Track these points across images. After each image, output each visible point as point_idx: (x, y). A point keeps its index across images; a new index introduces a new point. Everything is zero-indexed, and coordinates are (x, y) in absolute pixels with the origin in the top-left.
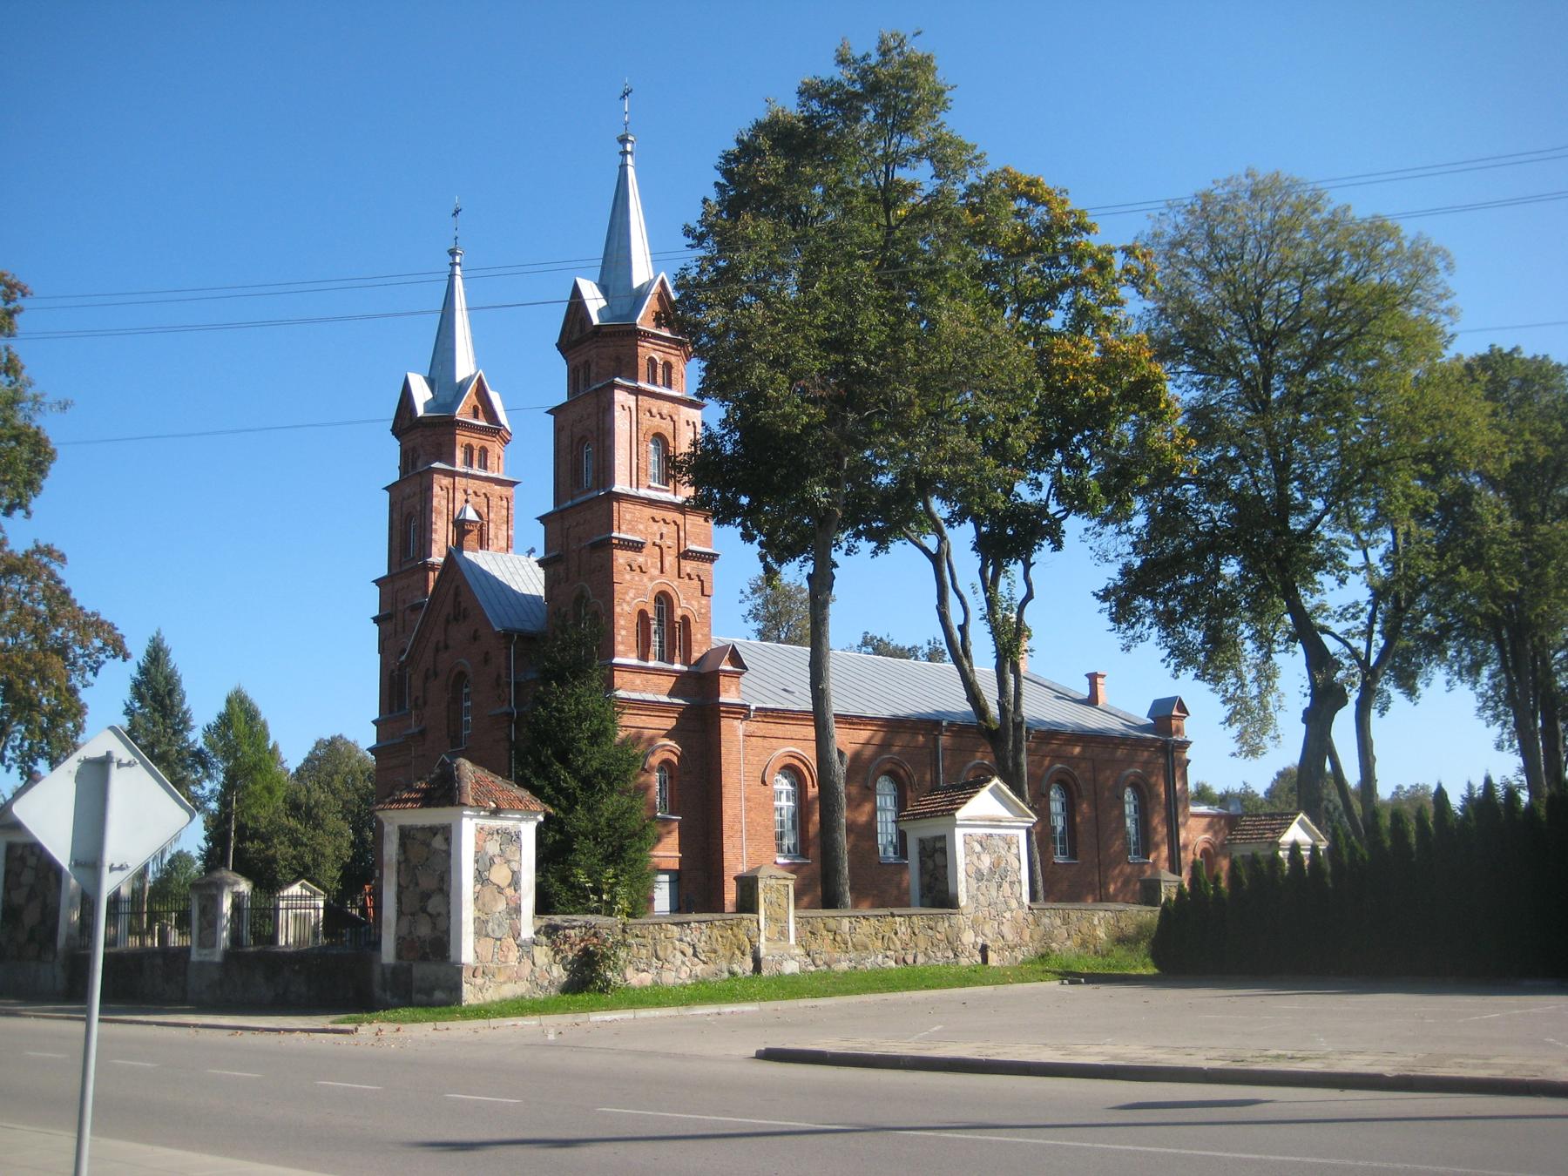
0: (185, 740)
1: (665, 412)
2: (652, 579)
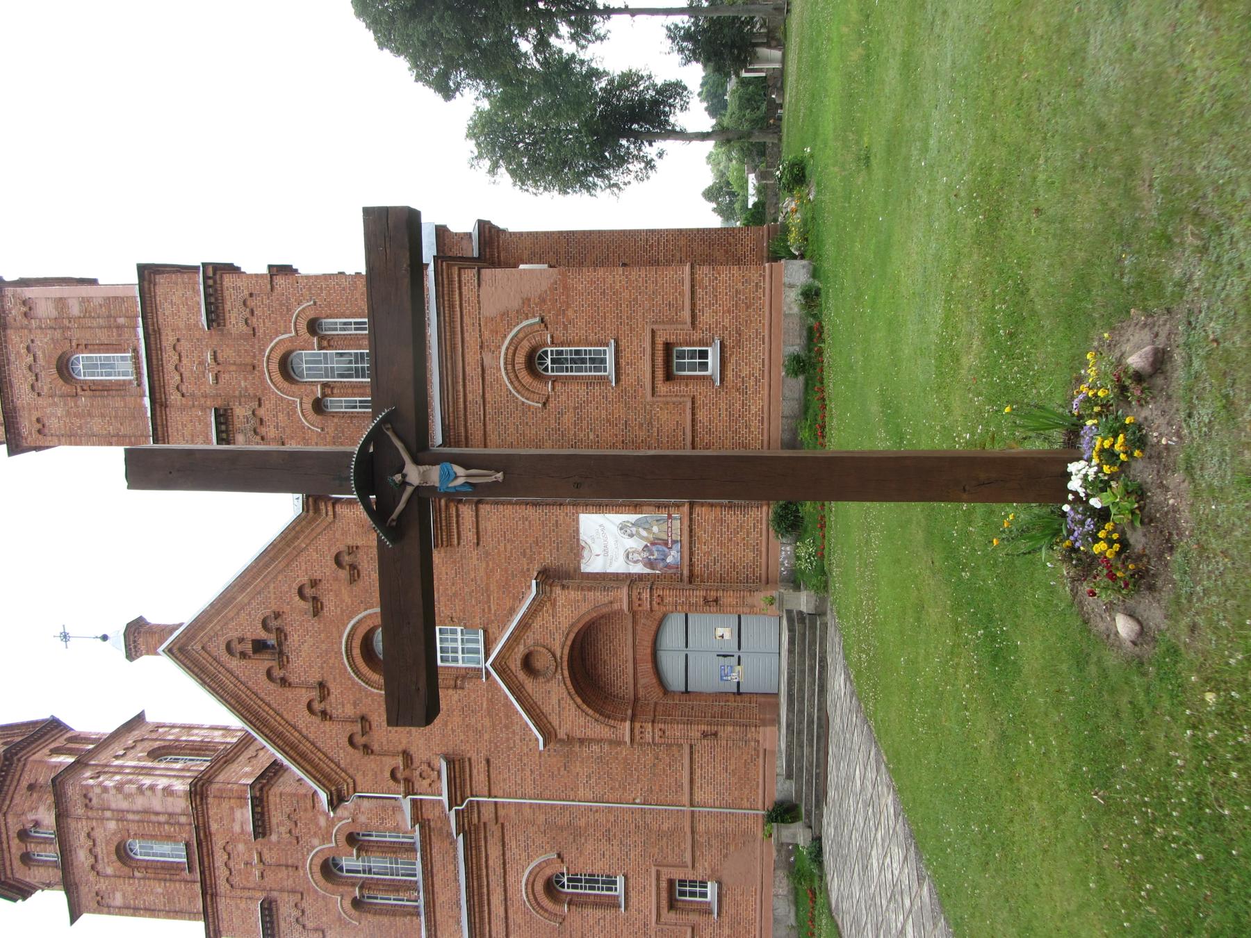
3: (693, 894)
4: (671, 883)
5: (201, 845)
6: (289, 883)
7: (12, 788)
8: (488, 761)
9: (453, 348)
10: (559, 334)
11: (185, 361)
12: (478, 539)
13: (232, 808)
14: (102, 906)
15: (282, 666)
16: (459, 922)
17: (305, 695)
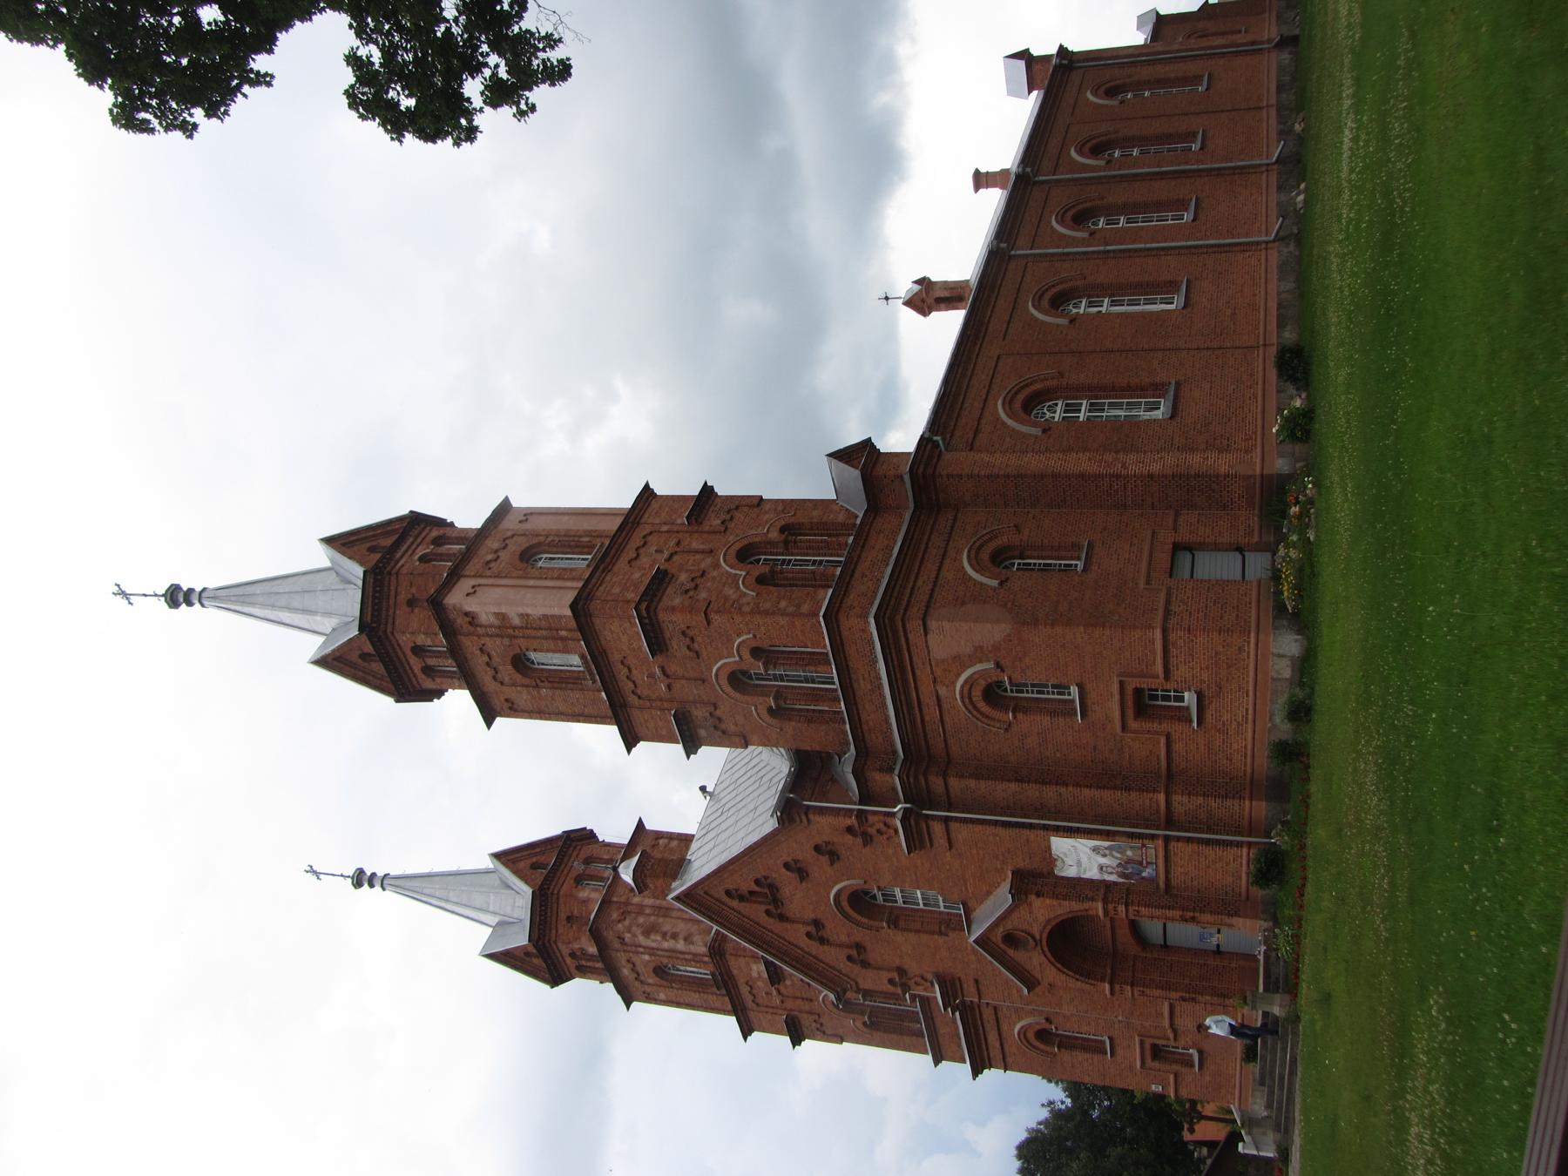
1: (496, 545)
2: (716, 565)
3: (1167, 698)
4: (1138, 692)
5: (598, 657)
6: (807, 1007)
8: (976, 981)
9: (905, 681)
10: (1017, 678)
11: (634, 672)
13: (748, 964)
14: (514, 711)
15: (777, 908)
16: (959, 1045)
17: (803, 929)
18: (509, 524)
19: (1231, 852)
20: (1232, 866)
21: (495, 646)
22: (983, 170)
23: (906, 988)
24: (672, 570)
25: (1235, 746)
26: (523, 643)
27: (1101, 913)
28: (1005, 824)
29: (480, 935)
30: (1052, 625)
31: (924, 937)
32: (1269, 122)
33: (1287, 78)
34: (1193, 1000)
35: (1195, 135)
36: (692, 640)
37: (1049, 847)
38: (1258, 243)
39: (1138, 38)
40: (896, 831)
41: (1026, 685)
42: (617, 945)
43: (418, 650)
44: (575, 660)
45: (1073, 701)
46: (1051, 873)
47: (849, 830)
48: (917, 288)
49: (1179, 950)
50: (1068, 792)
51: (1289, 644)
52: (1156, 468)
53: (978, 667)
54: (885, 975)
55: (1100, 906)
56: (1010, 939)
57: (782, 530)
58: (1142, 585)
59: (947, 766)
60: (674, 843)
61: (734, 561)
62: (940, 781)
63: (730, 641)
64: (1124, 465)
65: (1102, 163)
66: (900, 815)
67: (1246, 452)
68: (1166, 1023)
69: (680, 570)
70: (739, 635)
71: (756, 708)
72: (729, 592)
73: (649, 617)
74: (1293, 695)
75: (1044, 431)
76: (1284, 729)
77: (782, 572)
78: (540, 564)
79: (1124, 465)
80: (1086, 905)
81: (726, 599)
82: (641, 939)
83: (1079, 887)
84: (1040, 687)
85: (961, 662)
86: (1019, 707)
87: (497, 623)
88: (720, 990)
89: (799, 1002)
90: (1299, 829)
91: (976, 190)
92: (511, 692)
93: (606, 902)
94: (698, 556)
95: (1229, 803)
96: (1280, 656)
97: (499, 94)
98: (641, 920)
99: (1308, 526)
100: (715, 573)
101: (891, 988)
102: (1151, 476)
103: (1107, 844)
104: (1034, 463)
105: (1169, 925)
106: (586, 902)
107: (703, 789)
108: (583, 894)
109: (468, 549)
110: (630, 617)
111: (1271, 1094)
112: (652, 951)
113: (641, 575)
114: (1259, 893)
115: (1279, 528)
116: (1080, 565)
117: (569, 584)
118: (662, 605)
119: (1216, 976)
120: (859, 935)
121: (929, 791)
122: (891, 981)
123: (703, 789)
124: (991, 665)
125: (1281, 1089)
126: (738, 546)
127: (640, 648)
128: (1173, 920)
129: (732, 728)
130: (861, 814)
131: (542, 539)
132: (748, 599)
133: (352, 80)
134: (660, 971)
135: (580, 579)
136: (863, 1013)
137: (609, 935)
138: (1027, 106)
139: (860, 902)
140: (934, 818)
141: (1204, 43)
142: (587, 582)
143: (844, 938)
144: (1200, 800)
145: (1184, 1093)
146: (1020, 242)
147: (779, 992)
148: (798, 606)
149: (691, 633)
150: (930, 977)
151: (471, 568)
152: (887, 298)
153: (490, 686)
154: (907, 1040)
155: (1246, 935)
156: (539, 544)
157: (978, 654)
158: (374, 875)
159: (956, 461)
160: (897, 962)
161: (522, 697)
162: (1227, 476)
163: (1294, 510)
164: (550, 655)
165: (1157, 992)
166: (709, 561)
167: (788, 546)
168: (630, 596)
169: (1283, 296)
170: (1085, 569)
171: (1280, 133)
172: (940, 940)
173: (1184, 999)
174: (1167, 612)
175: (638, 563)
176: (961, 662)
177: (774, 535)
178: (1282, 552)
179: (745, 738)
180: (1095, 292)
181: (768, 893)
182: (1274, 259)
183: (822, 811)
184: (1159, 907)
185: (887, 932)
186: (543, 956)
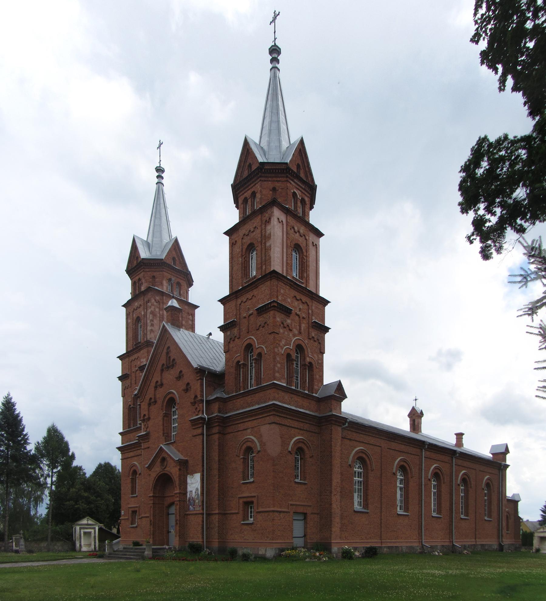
0: (25, 448)
1: (301, 231)
2: (294, 336)
4: (252, 502)
5: (255, 284)
7: (153, 270)
8: (149, 448)
12: (195, 436)
16: (127, 442)
17: (159, 380)
18: (312, 237)
19: (201, 536)
20: (196, 536)
21: (257, 233)
22: (463, 436)
23: (143, 421)
24: (291, 316)
25: (236, 536)
26: (259, 249)
27: (176, 492)
28: (203, 456)
29: (143, 234)
30: (273, 471)
31: (162, 427)
32: (469, 542)
33: (487, 548)
34: (151, 524)
35: (467, 516)
36: (263, 327)
37: (197, 473)
38: (422, 539)
39: (510, 493)
40: (197, 415)
41: (253, 462)
42: (146, 300)
43: (254, 194)
44: (254, 273)
45: (249, 479)
46: (188, 474)
47: (196, 397)
48: (419, 412)
49: (168, 519)
50: (216, 479)
51: (270, 553)
52: (334, 506)
53: (258, 444)
54: (146, 413)
55: (178, 491)
56: (164, 460)
57: (310, 363)
58: (290, 503)
59: (222, 434)
60: (190, 322)
61: (297, 343)
62: (217, 431)
63: (263, 343)
64: (336, 495)
65: (459, 482)
66: (203, 416)
67: (340, 537)
68: (143, 515)
69: (292, 320)
70: (266, 347)
71: (239, 356)
72: (283, 342)
73: (271, 307)
74: (251, 555)
75: (350, 465)
76: (240, 552)
77: (293, 364)
78: (294, 254)
79: (336, 495)
80: (178, 487)
81: (280, 341)
82: (149, 311)
83: (184, 484)
84: (253, 467)
85: (260, 438)
86: (245, 460)
87: (267, 234)
88: (135, 345)
89: (134, 379)
90: (208, 558)
91: (456, 434)
92: (239, 243)
93: (162, 294)
94: (298, 327)
95: (217, 534)
96: (266, 550)
97: (478, 223)
98: (157, 310)
99: (311, 559)
100: (291, 335)
101: (142, 415)
102: (331, 504)
103: (199, 493)
104: (337, 462)
105: (174, 515)
106: (162, 284)
107: (210, 334)
108: (165, 283)
109: (299, 217)
110: (271, 298)
111: (121, 551)
112: (145, 315)
113: (289, 303)
114: (187, 545)
115: (313, 549)
116: (297, 480)
117: (285, 269)
118: (276, 313)
119: (160, 532)
120: (159, 402)
121: (213, 427)
122: (145, 415)
123: (210, 334)
124: (259, 449)
125: (123, 555)
126: (303, 345)
127: (259, 304)
128: (176, 517)
129: (231, 346)
130: (203, 401)
131: (305, 254)
132: (280, 350)
133: (491, 141)
134: (138, 319)
135: (287, 273)
136: (134, 404)
137: (149, 295)
138: (485, 452)
139: (171, 402)
140: (203, 429)
141: (504, 519)
142: (286, 278)
143: (158, 396)
144: (217, 525)
145: (123, 522)
146: (428, 453)
147: (137, 370)
148: (278, 372)
149: (266, 326)
150: (148, 430)
151: (290, 219)
152: (416, 400)
153: (243, 231)
154: (127, 422)
155: (174, 541)
156: (303, 253)
157: (263, 444)
158: (162, 178)
159: (337, 432)
160: (152, 417)
161: (237, 249)
162: (331, 531)
163: (318, 554)
164: (255, 261)
165: (152, 512)
166: (296, 332)
167: (304, 366)
168: (280, 298)
169: (400, 548)
170: (296, 482)
171: (465, 546)
172: (161, 433)
173: (151, 521)
174: (280, 512)
175: (295, 300)
176: (260, 438)
177: (308, 360)
178: (303, 550)
179: (228, 351)
180: (406, 482)
181: (170, 365)
182: (415, 545)
183: (202, 385)
184: (180, 512)
185: (162, 413)
186: (137, 266)
